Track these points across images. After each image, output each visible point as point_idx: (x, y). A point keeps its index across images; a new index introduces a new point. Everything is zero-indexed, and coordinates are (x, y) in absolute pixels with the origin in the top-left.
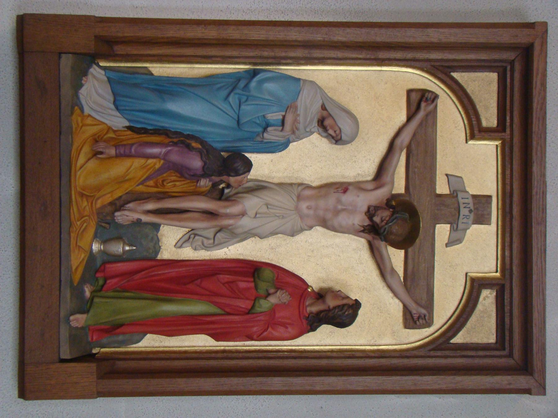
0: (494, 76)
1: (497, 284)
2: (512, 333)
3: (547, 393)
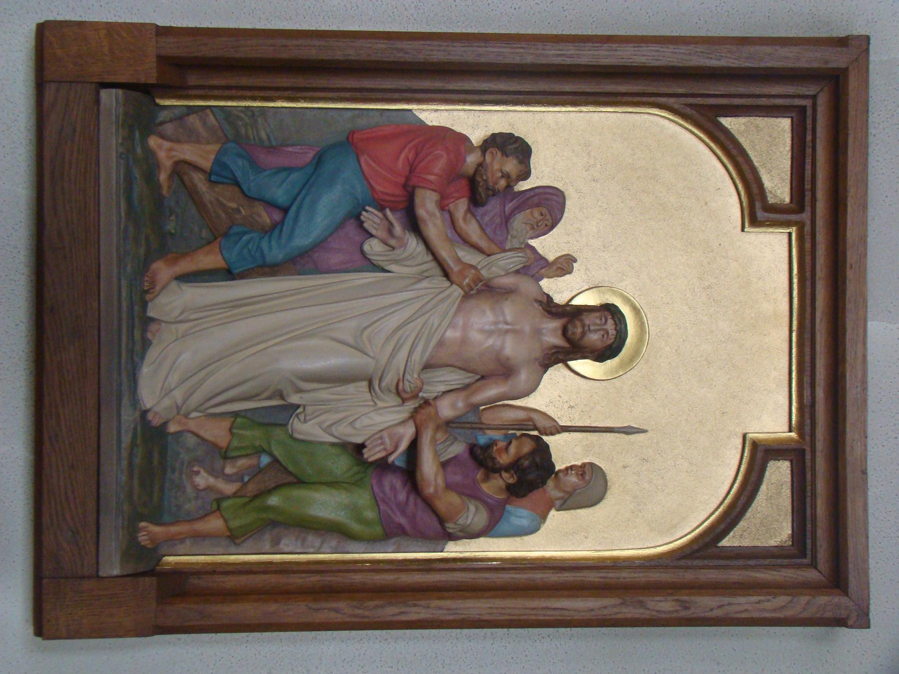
0: (785, 124)
1: (795, 450)
2: (815, 427)
3: (872, 621)
